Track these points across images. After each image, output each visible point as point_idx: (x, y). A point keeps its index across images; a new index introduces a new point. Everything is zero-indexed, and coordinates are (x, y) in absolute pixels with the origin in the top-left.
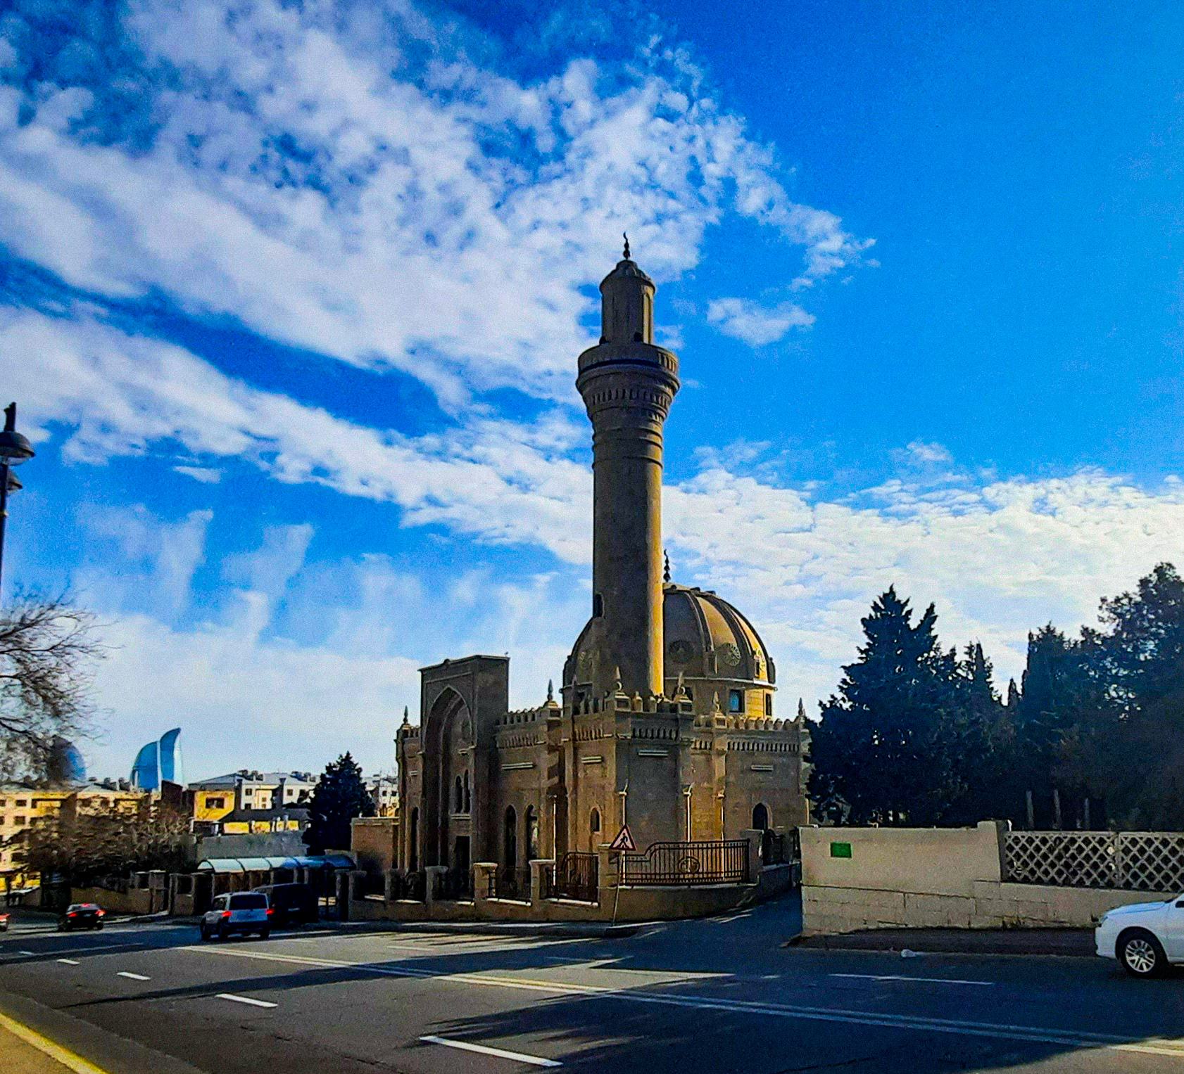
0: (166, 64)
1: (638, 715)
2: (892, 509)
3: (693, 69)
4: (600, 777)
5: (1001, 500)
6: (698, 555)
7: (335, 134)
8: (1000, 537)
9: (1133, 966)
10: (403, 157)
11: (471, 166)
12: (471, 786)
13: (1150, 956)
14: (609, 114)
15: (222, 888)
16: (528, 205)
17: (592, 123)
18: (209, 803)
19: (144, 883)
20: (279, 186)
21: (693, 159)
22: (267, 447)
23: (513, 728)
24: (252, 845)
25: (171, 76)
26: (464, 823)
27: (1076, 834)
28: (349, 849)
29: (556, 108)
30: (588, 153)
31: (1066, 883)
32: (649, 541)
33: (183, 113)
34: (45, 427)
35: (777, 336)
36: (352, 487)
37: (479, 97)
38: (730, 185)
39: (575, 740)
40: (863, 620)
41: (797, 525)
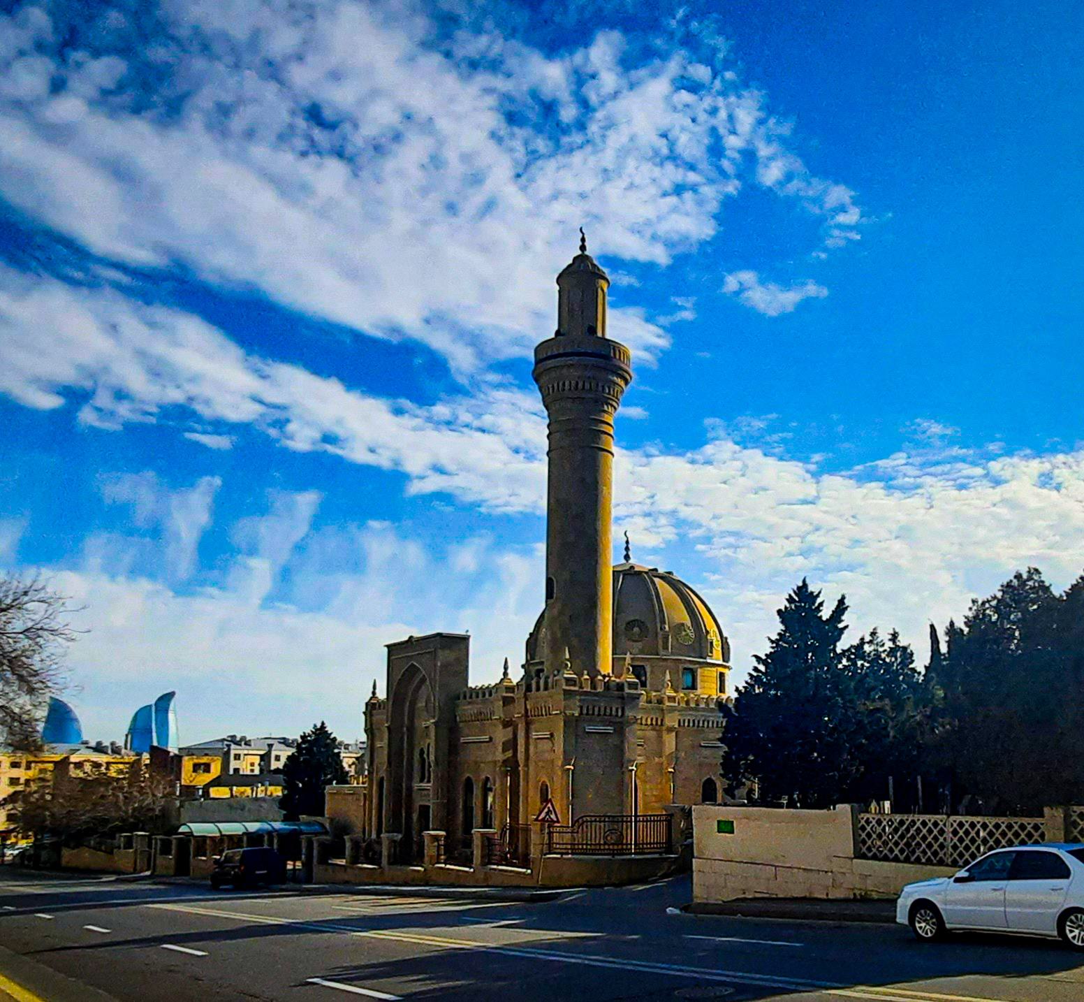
0: (196, 31)
1: (586, 693)
2: (900, 481)
3: (720, 42)
4: (548, 751)
5: (1006, 474)
6: (700, 526)
7: (362, 102)
8: (1003, 511)
9: (920, 932)
10: (428, 126)
11: (493, 135)
12: (432, 757)
13: (933, 923)
14: (632, 86)
15: (201, 850)
16: (548, 175)
17: (615, 95)
18: (196, 767)
19: (129, 844)
20: (304, 154)
21: (713, 131)
22: (278, 414)
23: (470, 703)
24: (234, 809)
25: (205, 45)
26: (426, 791)
27: (916, 817)
28: (323, 815)
29: (581, 78)
30: (610, 125)
31: (907, 860)
32: (600, 528)
33: (215, 83)
34: (59, 393)
35: (790, 309)
36: (359, 455)
37: (504, 67)
38: (749, 155)
39: (526, 715)
40: (779, 612)
41: (801, 497)
